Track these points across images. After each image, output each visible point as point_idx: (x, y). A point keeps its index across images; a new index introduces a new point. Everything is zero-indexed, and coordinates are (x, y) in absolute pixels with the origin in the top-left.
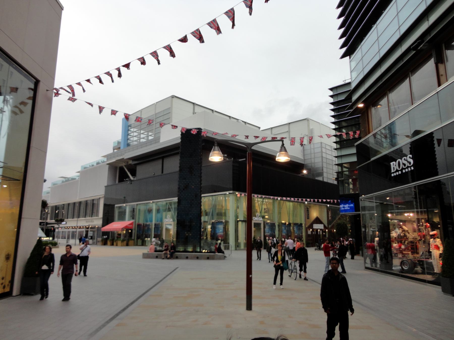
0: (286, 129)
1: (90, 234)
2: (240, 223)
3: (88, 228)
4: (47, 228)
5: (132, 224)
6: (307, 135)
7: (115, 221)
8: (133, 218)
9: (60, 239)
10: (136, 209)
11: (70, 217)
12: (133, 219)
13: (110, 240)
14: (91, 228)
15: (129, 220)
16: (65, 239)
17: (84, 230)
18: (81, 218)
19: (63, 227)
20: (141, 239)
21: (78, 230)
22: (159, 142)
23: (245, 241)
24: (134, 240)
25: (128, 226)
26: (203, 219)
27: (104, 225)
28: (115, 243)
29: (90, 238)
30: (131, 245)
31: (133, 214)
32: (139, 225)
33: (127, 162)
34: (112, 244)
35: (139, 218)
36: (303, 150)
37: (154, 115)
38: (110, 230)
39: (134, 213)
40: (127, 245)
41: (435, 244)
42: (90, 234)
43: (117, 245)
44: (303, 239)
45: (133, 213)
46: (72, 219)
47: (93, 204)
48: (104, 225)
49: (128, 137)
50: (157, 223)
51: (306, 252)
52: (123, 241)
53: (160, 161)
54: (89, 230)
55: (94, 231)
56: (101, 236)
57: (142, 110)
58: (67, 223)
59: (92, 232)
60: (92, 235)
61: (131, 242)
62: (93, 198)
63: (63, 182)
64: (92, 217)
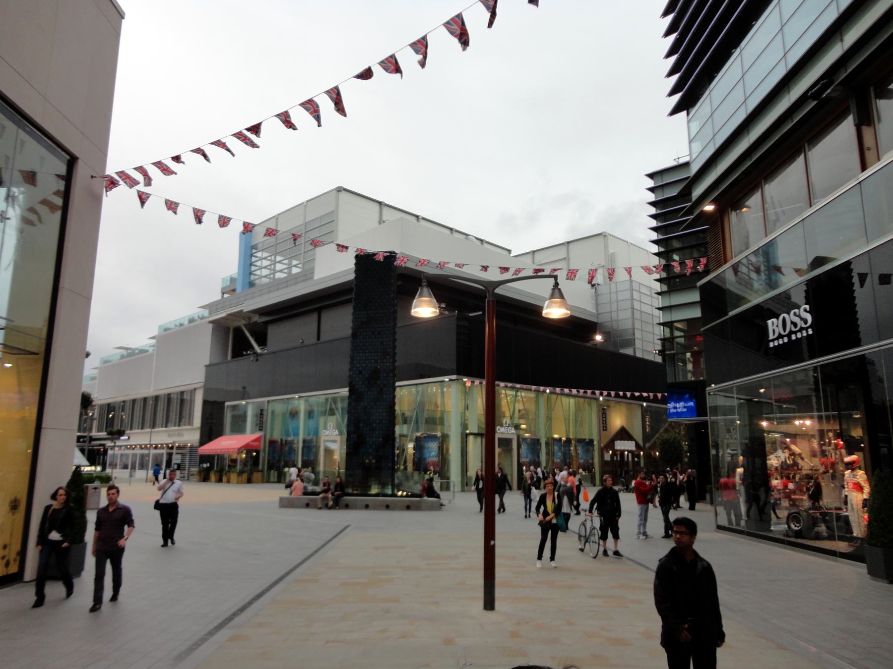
0: (561, 253)
6: (603, 266)
7: (225, 435)
8: (261, 428)
14: (179, 448)
15: (253, 432)
17: (164, 451)
22: (312, 278)
25: (250, 443)
27: (203, 442)
33: (250, 318)
37: (302, 225)
45: (260, 418)
47: (182, 401)
48: (203, 442)
53: (315, 317)
59: (179, 457)
63: (122, 357)
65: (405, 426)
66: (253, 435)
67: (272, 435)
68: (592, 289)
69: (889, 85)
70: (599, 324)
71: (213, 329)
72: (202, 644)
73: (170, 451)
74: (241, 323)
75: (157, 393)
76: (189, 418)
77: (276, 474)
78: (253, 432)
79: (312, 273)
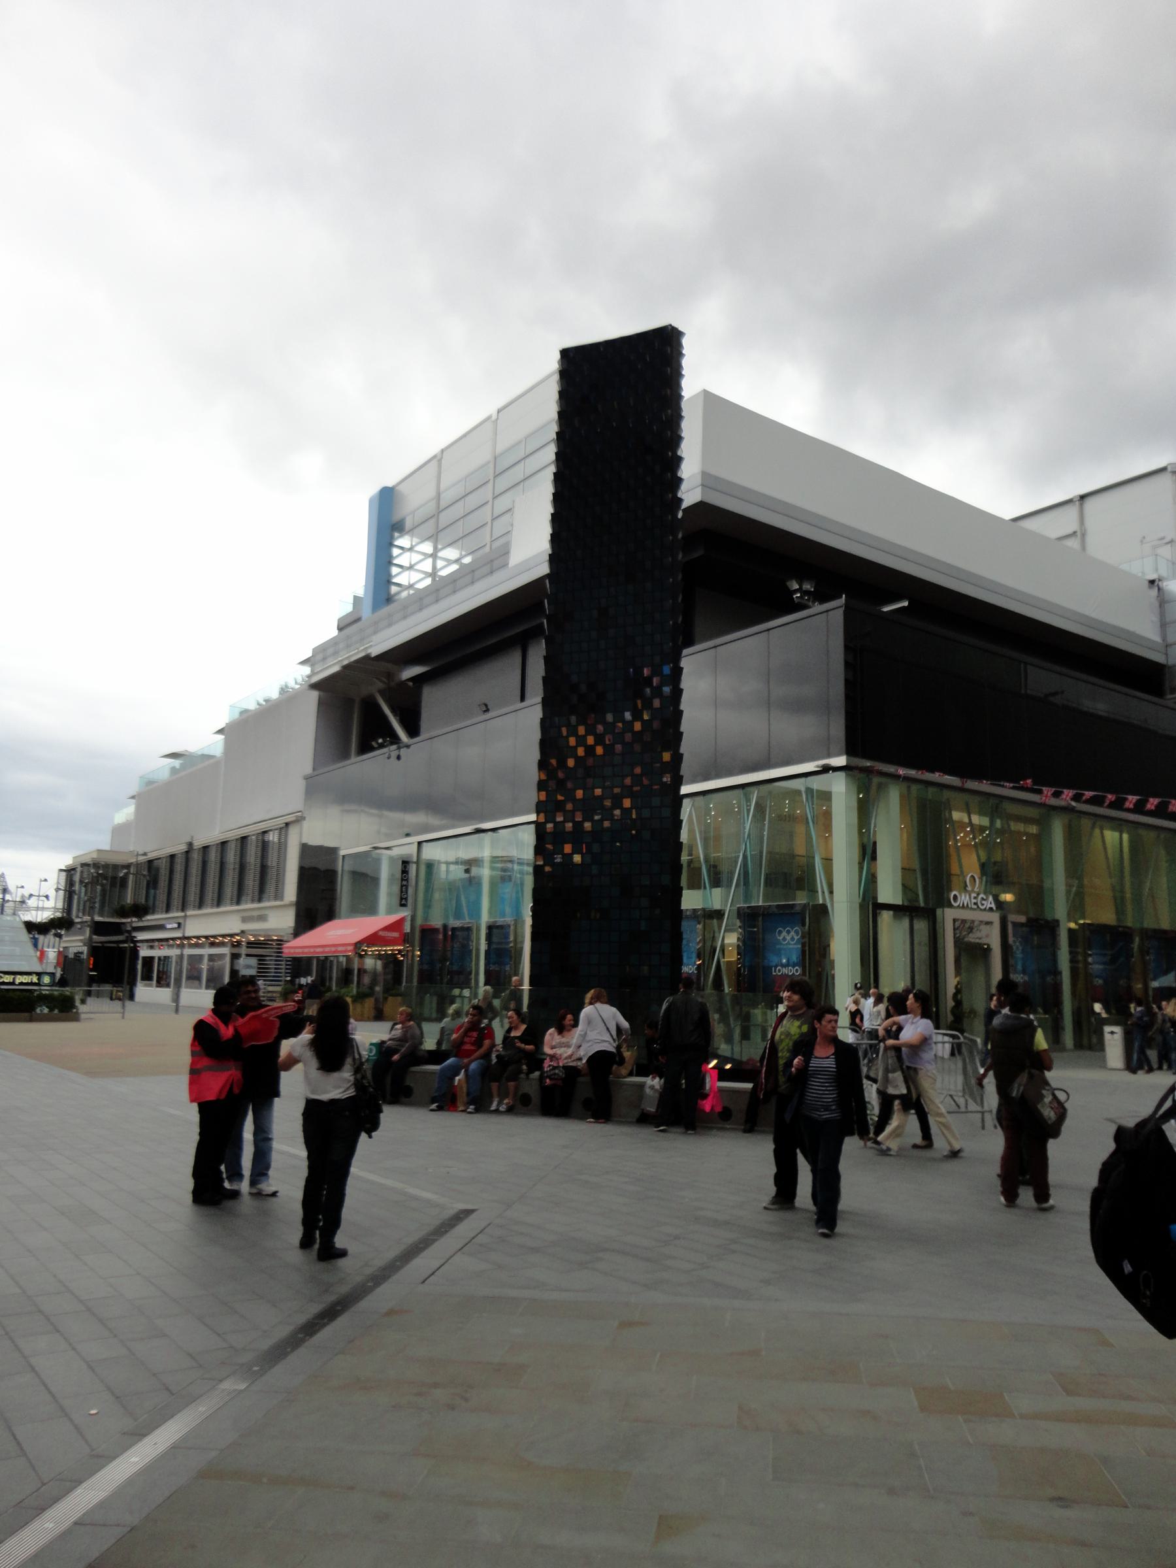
0: (1066, 522)
2: (886, 917)
3: (239, 943)
6: (1171, 541)
7: (340, 918)
8: (403, 902)
10: (417, 863)
12: (402, 905)
14: (250, 944)
15: (390, 911)
16: (168, 989)
17: (226, 950)
21: (207, 951)
22: (505, 565)
23: (406, 923)
25: (381, 933)
26: (691, 900)
27: (297, 933)
31: (402, 886)
32: (427, 933)
33: (390, 675)
35: (428, 906)
36: (1157, 604)
37: (488, 463)
39: (407, 880)
42: (248, 967)
44: (961, 997)
45: (402, 880)
46: (215, 910)
47: (264, 846)
48: (297, 933)
49: (613, 791)
50: (500, 921)
51: (859, 1001)
53: (515, 658)
55: (261, 958)
57: (444, 453)
59: (253, 961)
62: (263, 826)
63: (174, 770)
64: (260, 900)
65: (717, 892)
66: (389, 916)
67: (426, 919)
68: (1150, 588)
69: (1157, 642)
70: (1170, 667)
71: (321, 703)
72: (395, 1260)
73: (235, 951)
74: (374, 688)
75: (223, 838)
76: (277, 886)
77: (435, 999)
78: (390, 911)
79: (505, 552)
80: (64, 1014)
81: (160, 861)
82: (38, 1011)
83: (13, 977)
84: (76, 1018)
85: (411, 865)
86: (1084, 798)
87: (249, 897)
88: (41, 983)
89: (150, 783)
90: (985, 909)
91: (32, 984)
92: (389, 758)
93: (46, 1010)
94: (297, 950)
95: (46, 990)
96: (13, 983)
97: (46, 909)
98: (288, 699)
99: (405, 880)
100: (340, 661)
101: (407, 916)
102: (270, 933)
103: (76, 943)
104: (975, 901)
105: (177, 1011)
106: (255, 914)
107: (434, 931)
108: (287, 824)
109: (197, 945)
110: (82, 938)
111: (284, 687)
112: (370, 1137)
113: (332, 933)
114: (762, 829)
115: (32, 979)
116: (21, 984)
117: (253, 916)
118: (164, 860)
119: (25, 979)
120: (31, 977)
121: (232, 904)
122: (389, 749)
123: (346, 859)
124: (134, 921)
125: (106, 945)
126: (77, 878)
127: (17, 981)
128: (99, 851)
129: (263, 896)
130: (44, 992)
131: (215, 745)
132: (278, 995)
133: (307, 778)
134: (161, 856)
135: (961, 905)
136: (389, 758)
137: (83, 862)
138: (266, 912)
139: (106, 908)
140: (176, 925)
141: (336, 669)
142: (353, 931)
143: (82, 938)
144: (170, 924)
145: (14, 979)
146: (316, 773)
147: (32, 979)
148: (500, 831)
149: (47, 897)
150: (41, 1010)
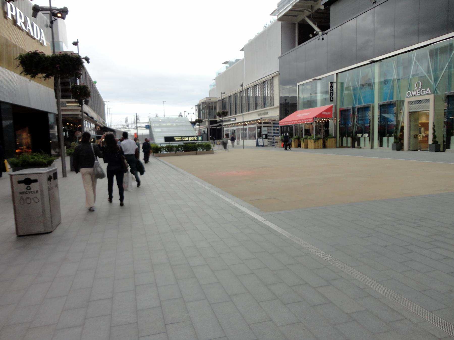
1: (264, 131)
3: (261, 123)
4: (211, 128)
5: (330, 110)
8: (332, 99)
9: (247, 139)
10: (337, 82)
11: (239, 112)
13: (295, 139)
14: (265, 123)
18: (238, 114)
19: (231, 124)
20: (349, 136)
24: (335, 137)
25: (323, 113)
28: (303, 144)
29: (264, 136)
30: (331, 147)
34: (299, 146)
38: (292, 122)
40: (324, 146)
41: (311, 130)
42: (264, 131)
43: (306, 147)
52: (317, 139)
54: (262, 125)
56: (280, 134)
58: (237, 119)
60: (266, 133)
61: (330, 142)
80: (208, 151)
81: (226, 99)
82: (199, 150)
83: (188, 138)
84: (212, 153)
85: (333, 83)
86: (34, 155)
87: (260, 107)
88: (198, 140)
89: (219, 74)
90: (425, 95)
91: (195, 140)
92: (319, 39)
93: (201, 150)
94: (286, 123)
95: (200, 143)
96: (188, 140)
97: (194, 118)
98: (268, 31)
99: (332, 90)
100: (291, 4)
101: (333, 105)
102: (271, 118)
103: (204, 128)
104: (419, 92)
105: (244, 148)
106: (263, 112)
107: (348, 110)
108: (273, 77)
109: (252, 124)
110: (205, 126)
111: (266, 25)
112: (49, 79)
113: (299, 115)
114: (214, 113)
115: (195, 138)
116: (191, 140)
117: (262, 113)
118: (227, 98)
119: (192, 139)
120: (194, 138)
121: (253, 110)
122: (319, 36)
123: (300, 86)
124: (224, 118)
125: (212, 128)
126: (201, 107)
127: (190, 140)
128: (207, 98)
129: (265, 105)
130: (200, 143)
131: (241, 56)
132: (279, 140)
133: (279, 58)
134: (267, 80)
135: (412, 96)
136: (319, 39)
137: (202, 102)
138: (267, 111)
139: (211, 117)
140: (234, 119)
141: (290, 8)
142: (309, 113)
143: (205, 126)
144: (232, 119)
145: (188, 139)
146: (283, 55)
147: (195, 138)
148: (382, 61)
149: (193, 113)
150: (200, 150)
